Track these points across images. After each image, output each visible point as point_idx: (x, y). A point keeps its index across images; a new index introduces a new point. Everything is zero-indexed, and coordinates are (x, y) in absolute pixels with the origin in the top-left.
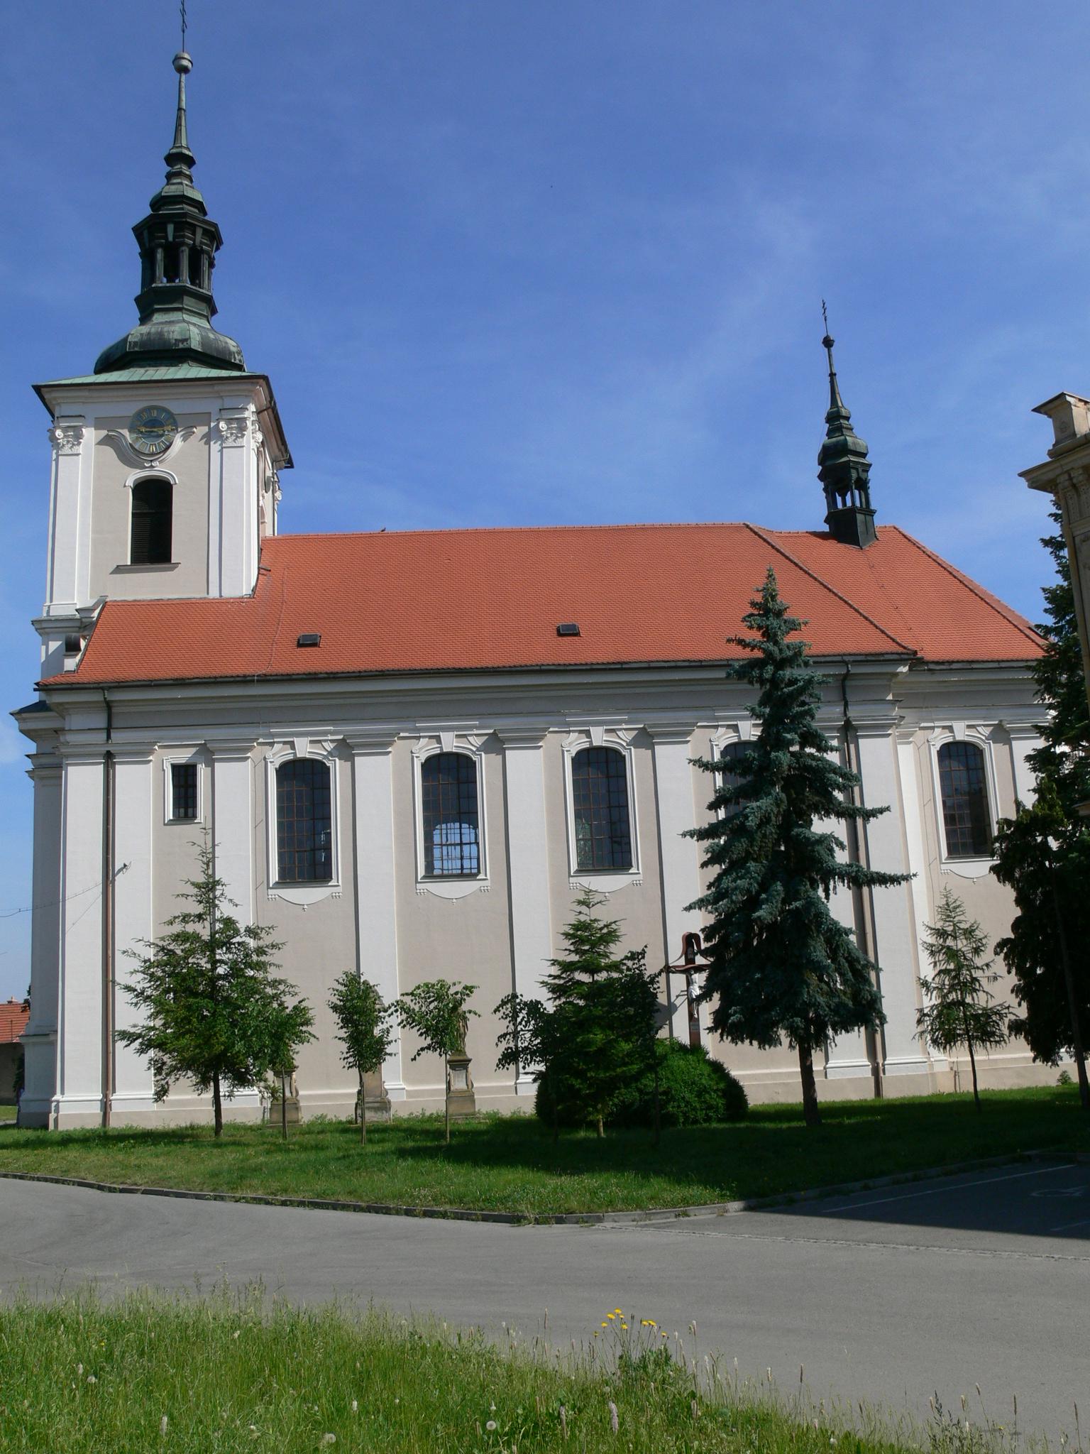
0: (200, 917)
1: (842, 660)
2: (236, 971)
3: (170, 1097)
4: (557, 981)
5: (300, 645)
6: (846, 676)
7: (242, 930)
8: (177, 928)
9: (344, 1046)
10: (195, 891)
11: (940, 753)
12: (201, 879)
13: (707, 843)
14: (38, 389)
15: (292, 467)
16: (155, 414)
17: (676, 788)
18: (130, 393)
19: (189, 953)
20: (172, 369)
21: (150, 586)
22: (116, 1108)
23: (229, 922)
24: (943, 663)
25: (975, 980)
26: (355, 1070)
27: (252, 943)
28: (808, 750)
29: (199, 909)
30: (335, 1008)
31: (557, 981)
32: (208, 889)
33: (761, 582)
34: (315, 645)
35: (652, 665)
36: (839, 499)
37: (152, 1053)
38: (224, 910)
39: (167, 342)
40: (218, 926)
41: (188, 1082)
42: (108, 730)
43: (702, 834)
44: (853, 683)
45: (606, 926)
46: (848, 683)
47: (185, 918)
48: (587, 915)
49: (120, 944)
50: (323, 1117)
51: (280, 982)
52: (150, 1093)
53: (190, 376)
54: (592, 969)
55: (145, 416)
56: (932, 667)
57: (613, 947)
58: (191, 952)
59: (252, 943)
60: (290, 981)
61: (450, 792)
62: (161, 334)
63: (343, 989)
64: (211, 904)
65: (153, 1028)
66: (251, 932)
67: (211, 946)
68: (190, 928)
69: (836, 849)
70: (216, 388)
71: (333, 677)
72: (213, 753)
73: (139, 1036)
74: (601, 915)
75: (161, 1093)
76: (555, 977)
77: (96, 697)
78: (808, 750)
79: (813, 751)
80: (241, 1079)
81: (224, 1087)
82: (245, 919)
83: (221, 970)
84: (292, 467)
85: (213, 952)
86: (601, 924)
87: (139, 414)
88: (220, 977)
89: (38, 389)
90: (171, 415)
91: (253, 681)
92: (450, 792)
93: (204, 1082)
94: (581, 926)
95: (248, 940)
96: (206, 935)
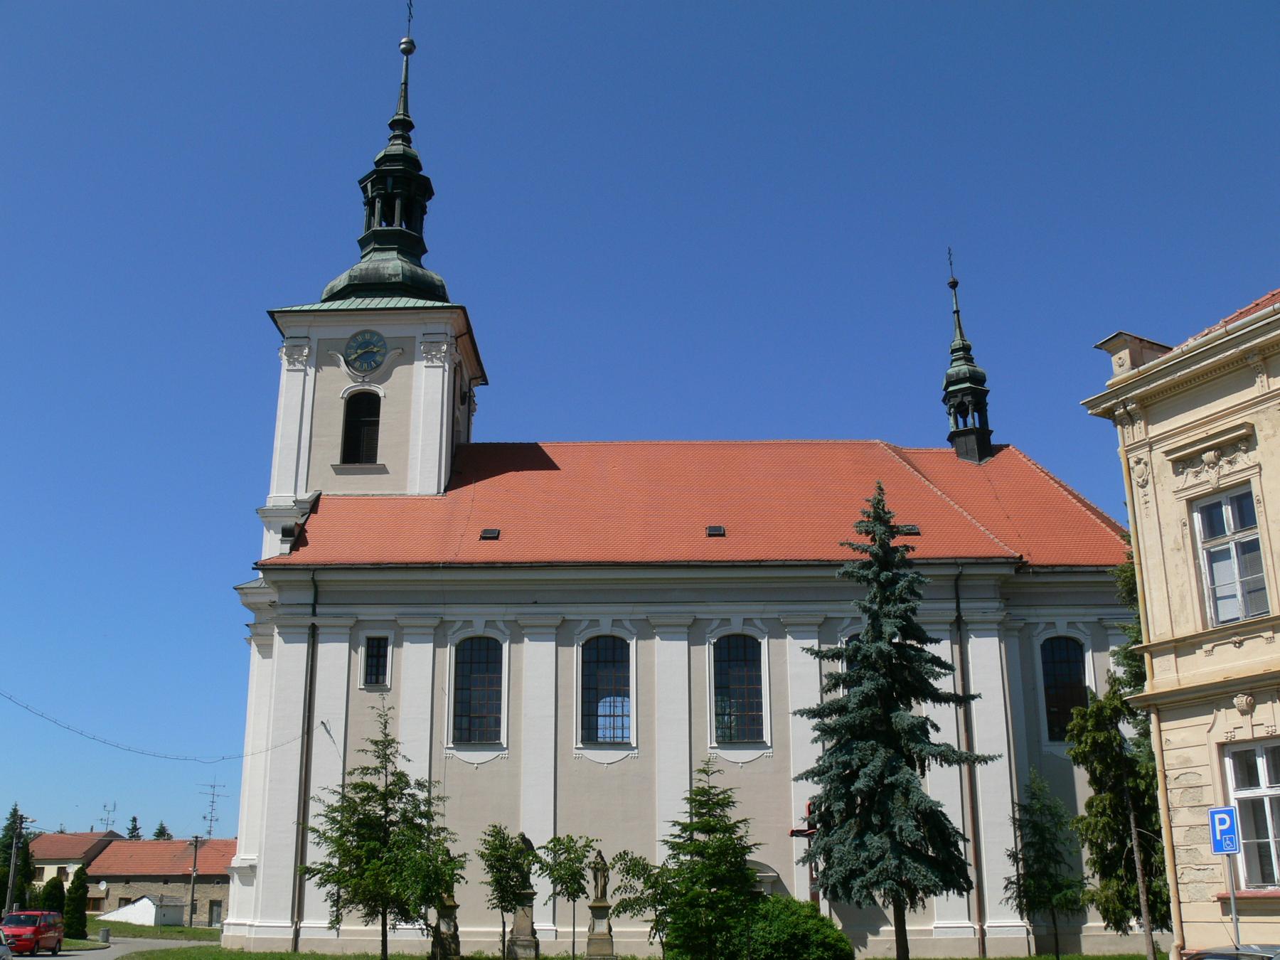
0: (377, 771)
1: (955, 562)
2: (406, 819)
3: (343, 927)
4: (677, 840)
5: (483, 538)
6: (958, 578)
7: (412, 783)
8: (356, 779)
9: (489, 890)
10: (373, 748)
11: (1043, 647)
12: (380, 737)
13: (816, 721)
14: (271, 314)
15: (487, 384)
16: (367, 336)
17: (796, 674)
18: (437, 316)
19: (366, 800)
20: (386, 300)
21: (358, 484)
22: (303, 935)
23: (401, 778)
24: (1047, 566)
25: (1058, 853)
26: (498, 911)
27: (422, 795)
28: (908, 642)
29: (376, 763)
30: (482, 856)
31: (677, 840)
32: (385, 747)
33: (872, 494)
34: (496, 538)
35: (959, 561)
36: (960, 420)
37: (329, 887)
38: (401, 765)
39: (381, 276)
40: (390, 779)
41: (359, 914)
42: (314, 606)
43: (812, 713)
44: (970, 583)
45: (722, 793)
46: (961, 583)
47: (365, 770)
48: (702, 782)
49: (314, 791)
50: (481, 953)
51: (444, 829)
52: (326, 923)
53: (381, 306)
54: (708, 830)
55: (360, 339)
56: (1037, 569)
57: (728, 812)
58: (366, 800)
59: (422, 795)
60: (451, 829)
61: (605, 671)
62: (377, 269)
63: (490, 839)
64: (385, 758)
65: (330, 865)
66: (420, 785)
67: (386, 796)
68: (369, 779)
69: (931, 730)
70: (421, 316)
71: (507, 566)
72: (402, 628)
73: (319, 872)
74: (719, 783)
75: (336, 921)
76: (676, 837)
77: (307, 577)
78: (908, 642)
79: (914, 643)
80: (406, 916)
81: (390, 918)
82: (416, 770)
83: (393, 817)
84: (487, 384)
85: (385, 801)
86: (718, 791)
87: (354, 337)
88: (392, 823)
89: (271, 314)
90: (381, 338)
91: (438, 568)
92: (605, 671)
93: (370, 915)
94: (703, 792)
95: (417, 792)
96: (381, 788)
